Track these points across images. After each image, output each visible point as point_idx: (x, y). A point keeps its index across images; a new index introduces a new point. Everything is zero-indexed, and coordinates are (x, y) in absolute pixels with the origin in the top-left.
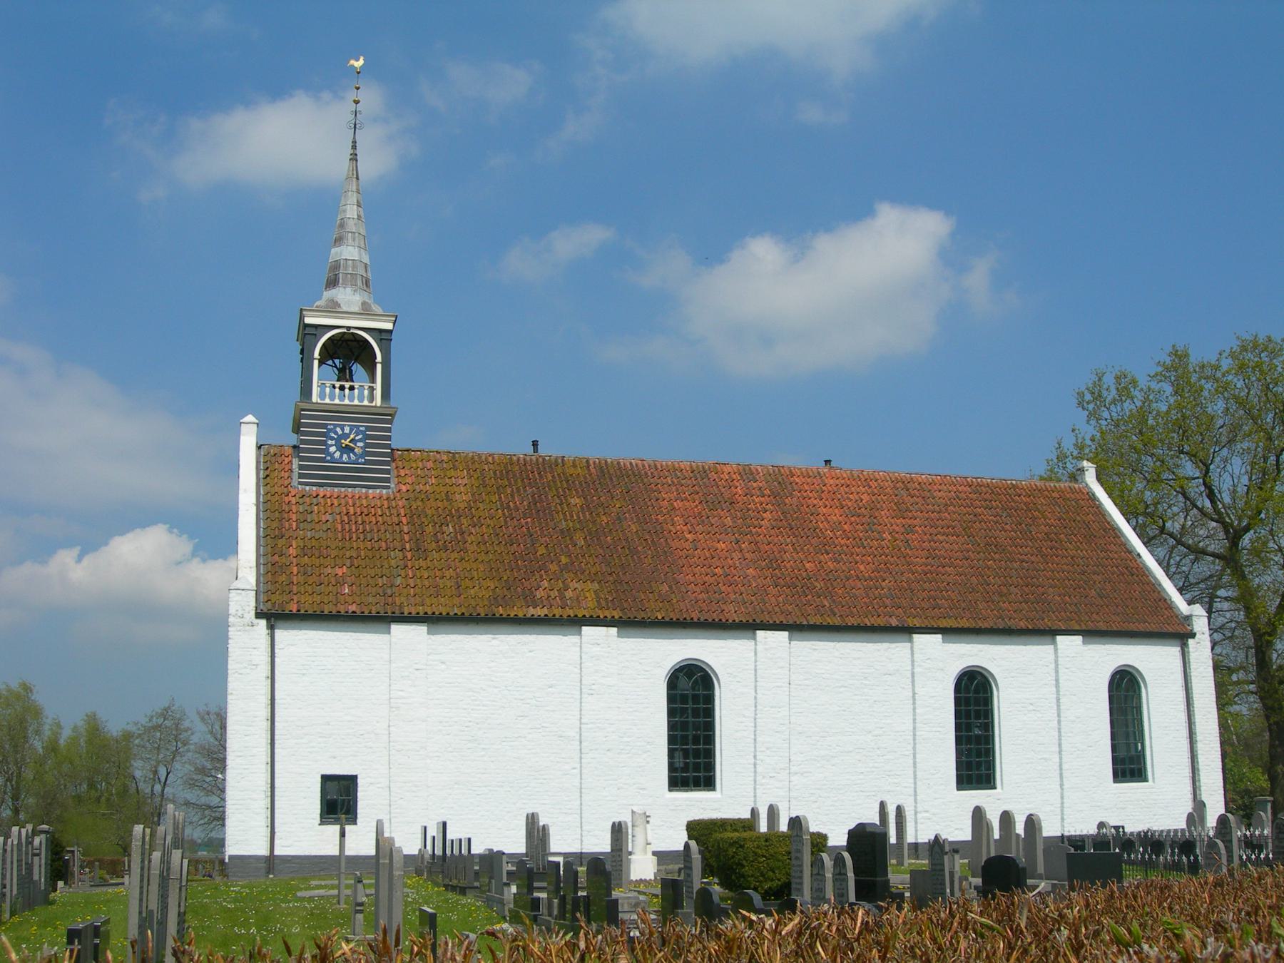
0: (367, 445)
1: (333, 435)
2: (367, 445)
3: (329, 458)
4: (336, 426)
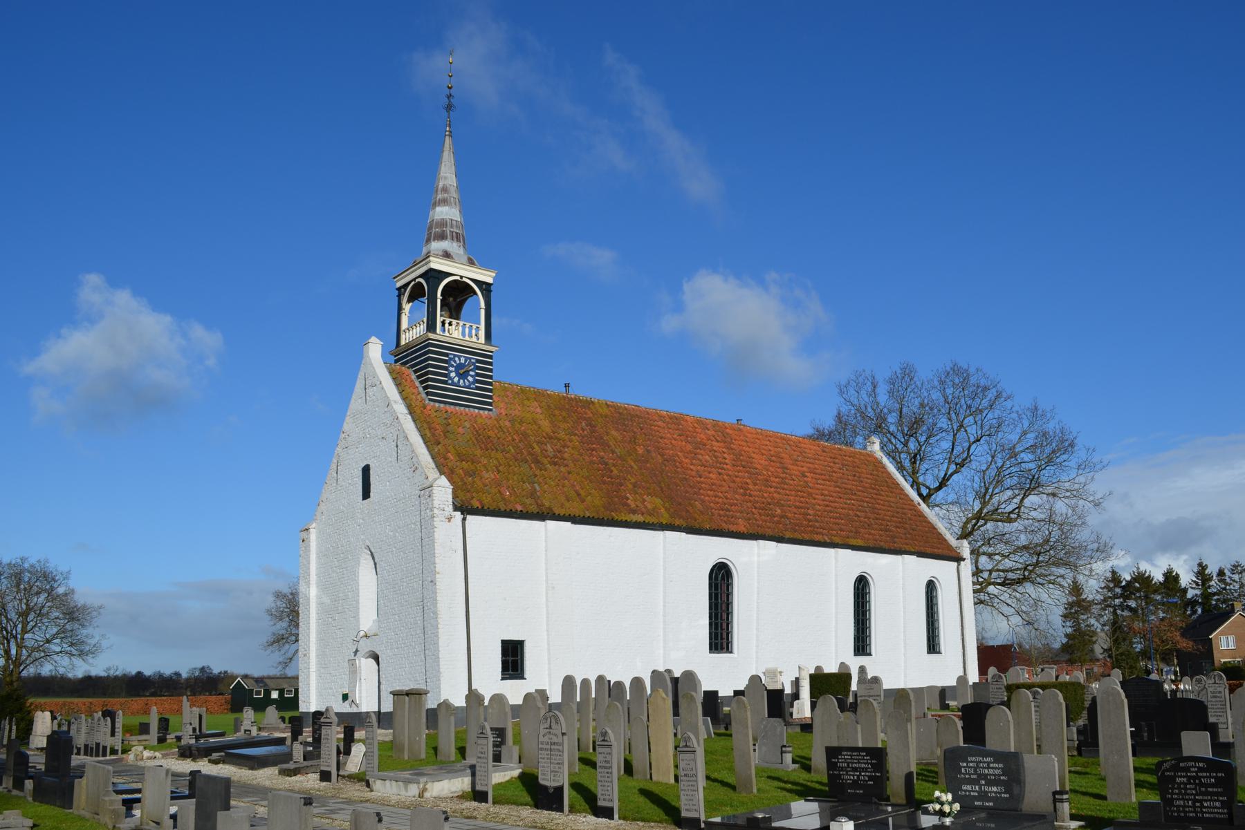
0: (478, 375)
1: (453, 363)
2: (478, 375)
3: (450, 382)
4: (455, 356)
